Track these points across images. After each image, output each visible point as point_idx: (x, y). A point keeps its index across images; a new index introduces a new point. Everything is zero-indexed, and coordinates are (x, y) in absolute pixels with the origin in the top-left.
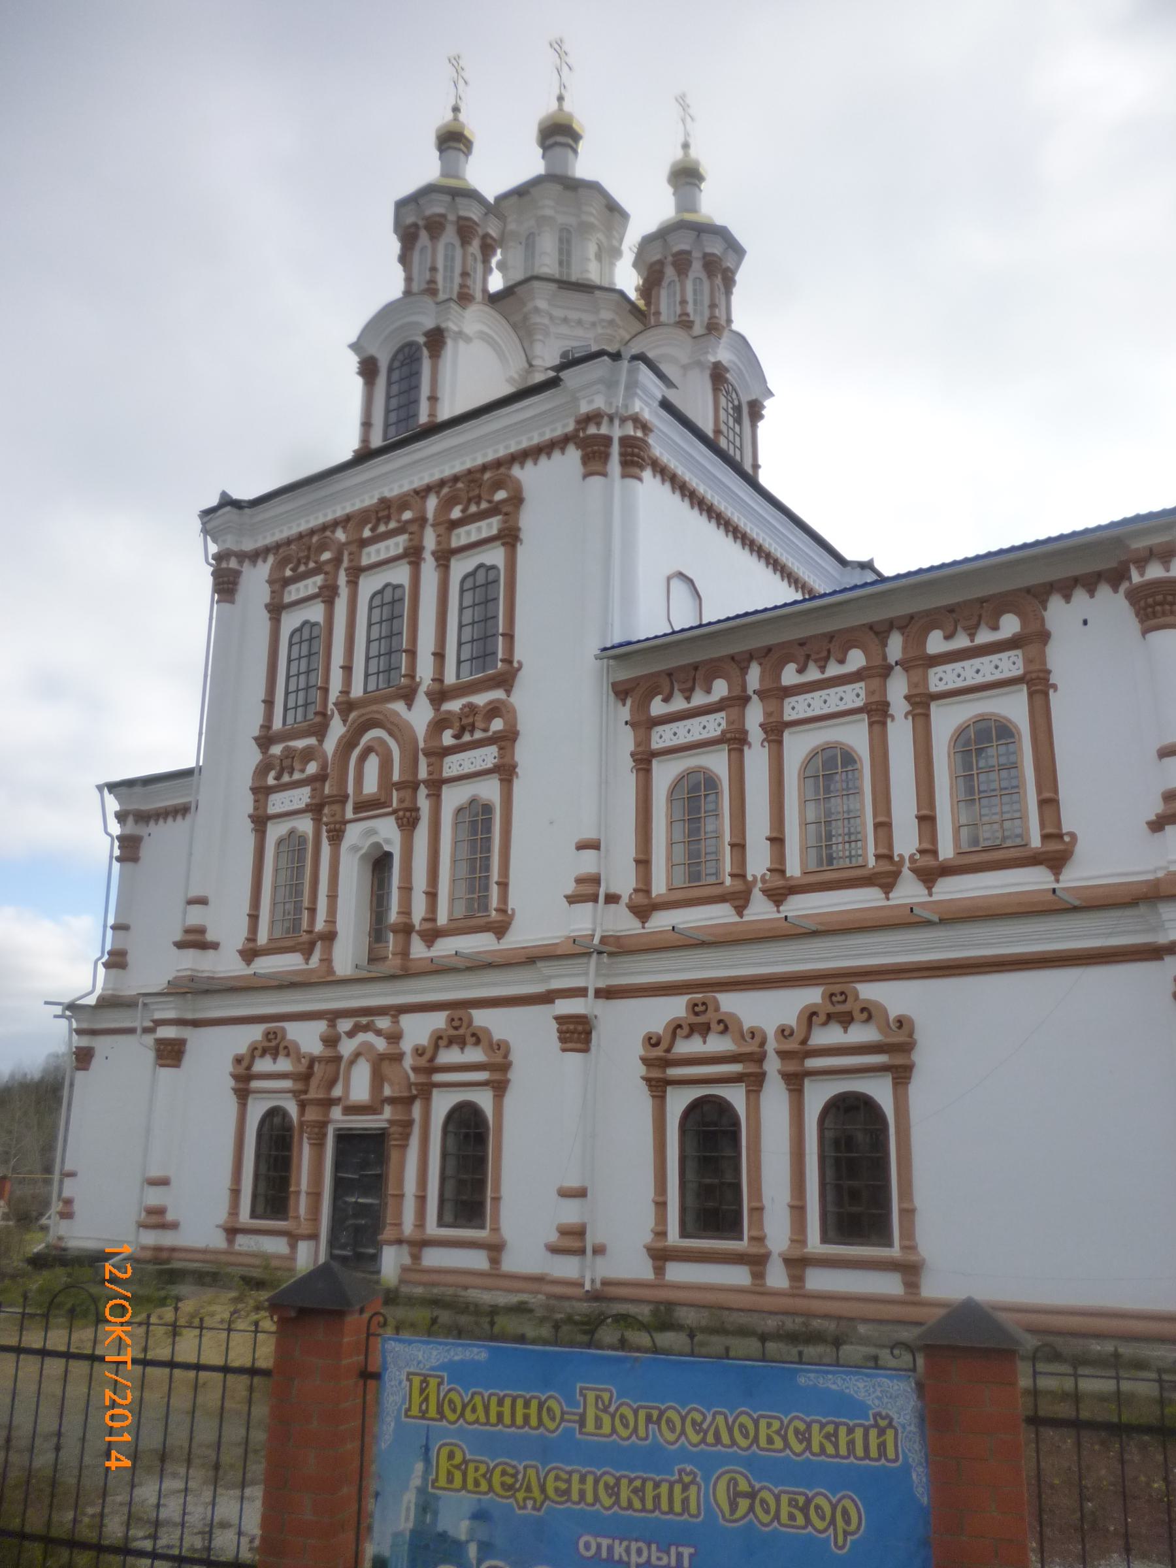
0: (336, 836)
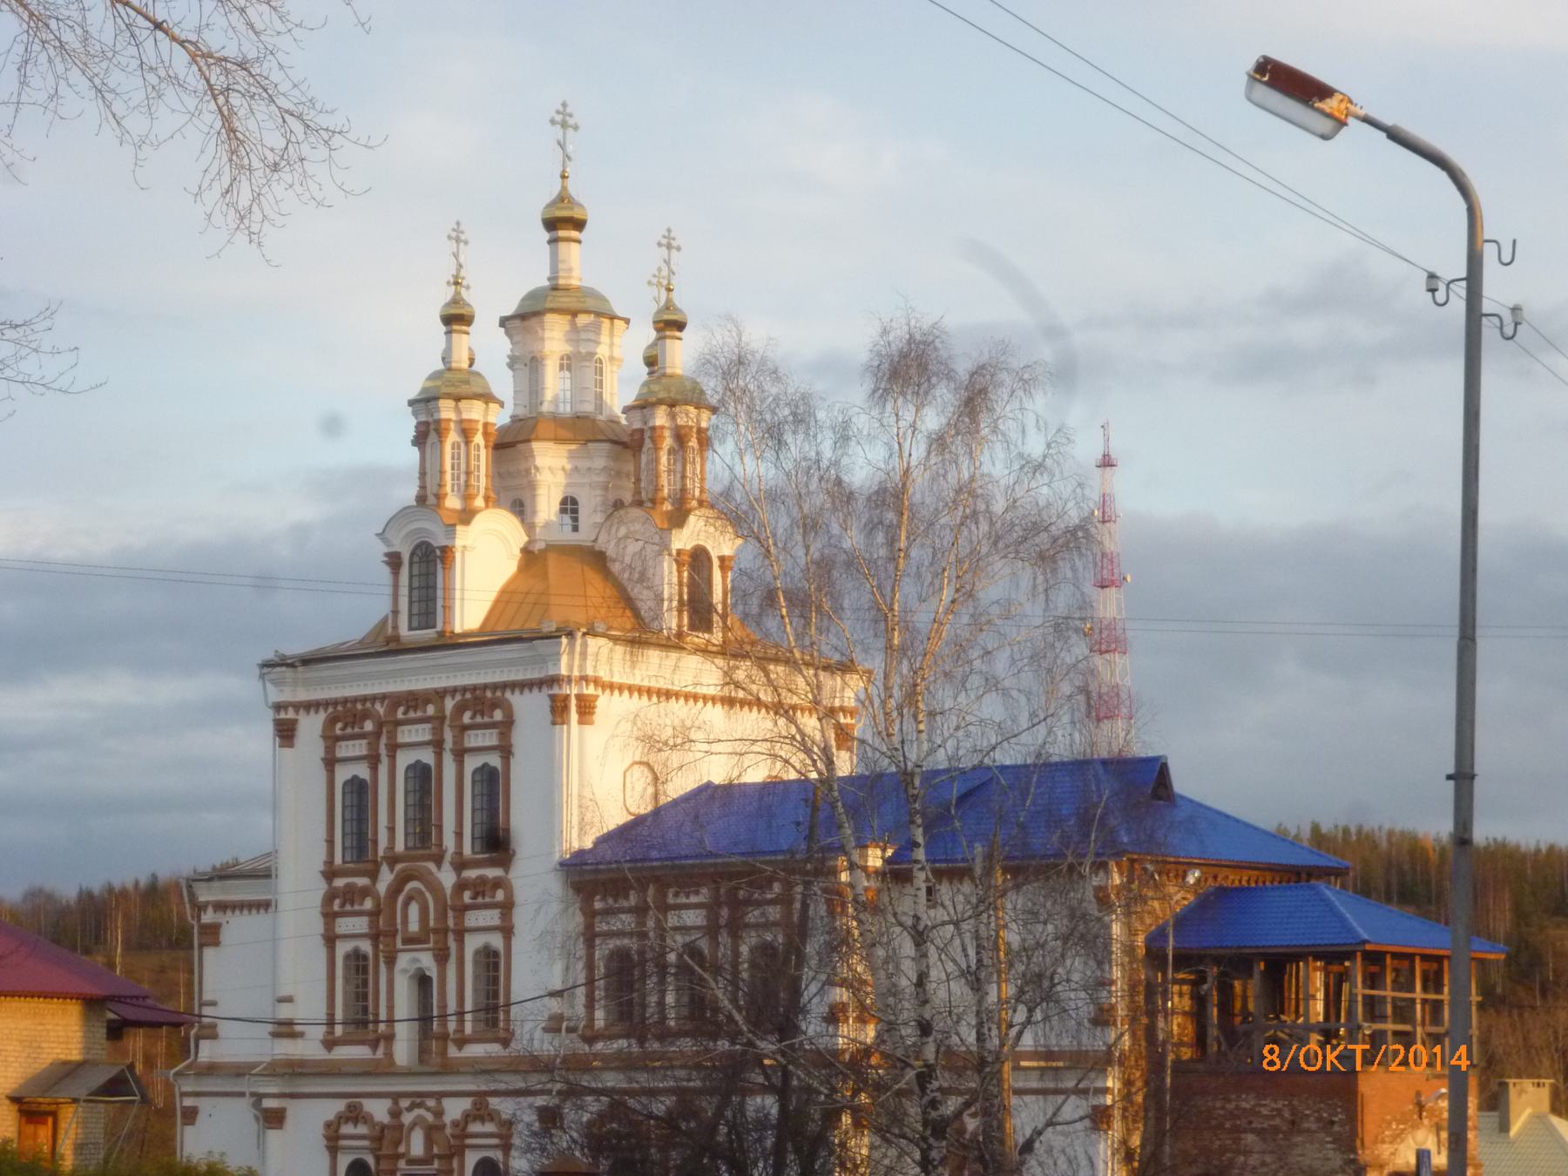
0: (391, 962)
